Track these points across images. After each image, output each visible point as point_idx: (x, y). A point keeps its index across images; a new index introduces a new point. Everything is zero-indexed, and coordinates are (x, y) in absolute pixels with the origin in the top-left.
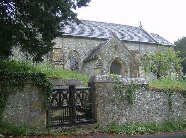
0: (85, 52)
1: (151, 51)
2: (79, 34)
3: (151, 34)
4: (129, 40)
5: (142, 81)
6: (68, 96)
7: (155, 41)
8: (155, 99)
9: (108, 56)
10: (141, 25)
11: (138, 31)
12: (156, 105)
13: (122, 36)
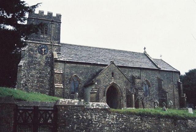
0: (85, 78)
1: (154, 77)
2: (81, 60)
3: (154, 59)
4: (130, 66)
5: (103, 106)
6: (33, 115)
7: (157, 67)
8: (116, 123)
9: (104, 81)
10: (146, 51)
11: (141, 57)
12: (117, 128)
13: (123, 62)
